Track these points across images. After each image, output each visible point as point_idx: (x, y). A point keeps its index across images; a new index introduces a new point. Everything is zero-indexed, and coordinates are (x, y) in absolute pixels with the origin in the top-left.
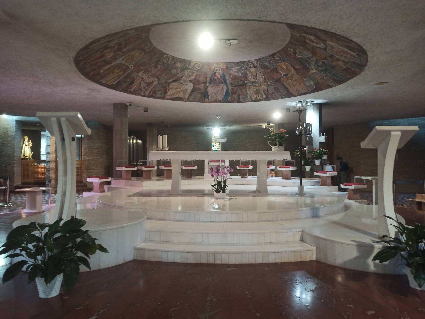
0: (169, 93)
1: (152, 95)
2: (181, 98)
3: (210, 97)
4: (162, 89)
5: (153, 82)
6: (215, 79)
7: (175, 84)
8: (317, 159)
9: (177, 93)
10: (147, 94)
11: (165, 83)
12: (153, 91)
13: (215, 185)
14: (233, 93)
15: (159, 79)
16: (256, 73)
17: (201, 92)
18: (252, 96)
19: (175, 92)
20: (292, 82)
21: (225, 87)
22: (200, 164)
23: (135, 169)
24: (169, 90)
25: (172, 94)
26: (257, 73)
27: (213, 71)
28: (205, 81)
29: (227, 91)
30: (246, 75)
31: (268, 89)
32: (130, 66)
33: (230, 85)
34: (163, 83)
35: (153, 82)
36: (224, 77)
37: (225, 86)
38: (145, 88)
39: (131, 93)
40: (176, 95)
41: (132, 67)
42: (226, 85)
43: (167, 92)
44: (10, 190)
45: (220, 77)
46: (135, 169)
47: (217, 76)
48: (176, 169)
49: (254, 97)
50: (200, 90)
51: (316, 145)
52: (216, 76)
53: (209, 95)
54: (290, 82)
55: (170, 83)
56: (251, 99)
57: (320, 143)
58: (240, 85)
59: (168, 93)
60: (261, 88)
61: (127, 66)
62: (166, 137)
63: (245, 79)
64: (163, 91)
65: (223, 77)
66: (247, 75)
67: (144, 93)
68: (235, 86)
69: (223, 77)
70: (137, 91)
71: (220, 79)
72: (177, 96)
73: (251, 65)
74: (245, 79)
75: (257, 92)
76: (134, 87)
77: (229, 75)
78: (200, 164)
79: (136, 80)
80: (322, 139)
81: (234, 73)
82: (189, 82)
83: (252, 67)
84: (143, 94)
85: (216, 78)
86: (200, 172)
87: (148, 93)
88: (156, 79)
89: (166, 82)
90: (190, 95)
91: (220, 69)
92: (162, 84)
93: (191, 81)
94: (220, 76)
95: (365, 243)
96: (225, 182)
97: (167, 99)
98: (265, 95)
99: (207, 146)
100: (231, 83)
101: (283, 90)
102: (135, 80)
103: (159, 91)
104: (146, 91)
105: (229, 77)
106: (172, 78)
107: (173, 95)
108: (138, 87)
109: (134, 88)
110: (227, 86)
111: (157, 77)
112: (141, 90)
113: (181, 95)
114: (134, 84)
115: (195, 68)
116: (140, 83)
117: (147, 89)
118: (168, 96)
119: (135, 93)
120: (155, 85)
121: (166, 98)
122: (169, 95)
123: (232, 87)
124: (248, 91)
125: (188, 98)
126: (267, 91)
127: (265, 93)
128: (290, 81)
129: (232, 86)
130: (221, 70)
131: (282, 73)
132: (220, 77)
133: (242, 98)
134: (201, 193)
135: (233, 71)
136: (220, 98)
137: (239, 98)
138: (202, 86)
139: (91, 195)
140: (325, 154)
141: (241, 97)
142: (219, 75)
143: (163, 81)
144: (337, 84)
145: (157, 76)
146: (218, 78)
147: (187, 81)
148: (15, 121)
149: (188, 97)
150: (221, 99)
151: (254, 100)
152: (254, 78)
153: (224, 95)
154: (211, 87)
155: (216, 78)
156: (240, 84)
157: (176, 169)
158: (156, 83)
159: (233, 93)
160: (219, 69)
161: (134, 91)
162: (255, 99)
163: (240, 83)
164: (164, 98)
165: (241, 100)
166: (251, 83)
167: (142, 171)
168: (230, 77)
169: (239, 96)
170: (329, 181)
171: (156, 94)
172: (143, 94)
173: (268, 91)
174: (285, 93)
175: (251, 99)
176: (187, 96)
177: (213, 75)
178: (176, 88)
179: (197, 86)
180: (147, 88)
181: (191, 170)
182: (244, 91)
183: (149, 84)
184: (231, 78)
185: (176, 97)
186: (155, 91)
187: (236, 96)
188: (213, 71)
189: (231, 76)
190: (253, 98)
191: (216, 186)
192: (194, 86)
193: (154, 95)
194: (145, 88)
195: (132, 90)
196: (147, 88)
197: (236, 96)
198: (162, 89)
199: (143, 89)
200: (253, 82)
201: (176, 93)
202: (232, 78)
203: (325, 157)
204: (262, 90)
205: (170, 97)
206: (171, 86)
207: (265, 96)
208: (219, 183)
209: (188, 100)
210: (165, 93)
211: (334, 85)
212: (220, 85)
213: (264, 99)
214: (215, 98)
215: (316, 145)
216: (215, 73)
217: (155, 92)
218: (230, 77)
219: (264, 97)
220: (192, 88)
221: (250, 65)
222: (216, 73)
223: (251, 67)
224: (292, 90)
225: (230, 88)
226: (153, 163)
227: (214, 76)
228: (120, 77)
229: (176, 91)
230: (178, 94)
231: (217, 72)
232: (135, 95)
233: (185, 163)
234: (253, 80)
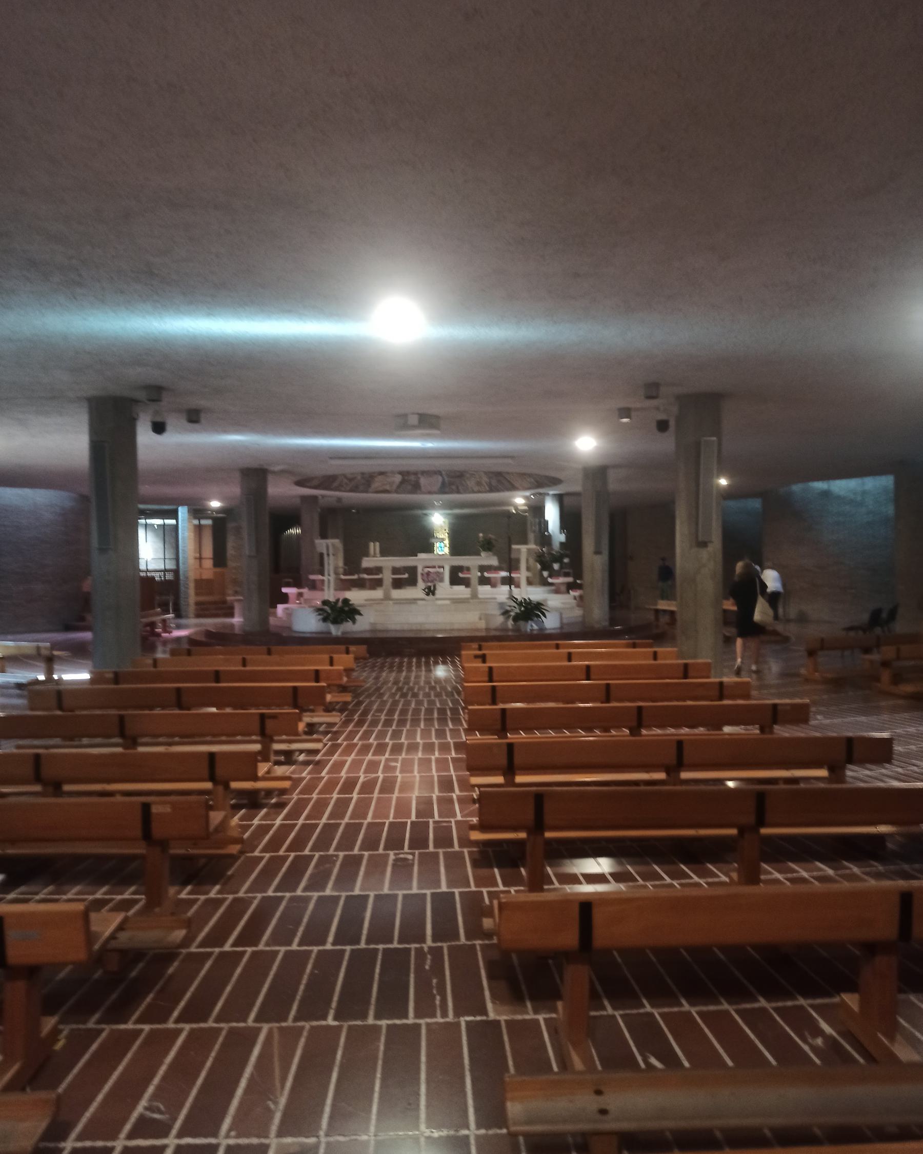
8: (556, 561)
13: (425, 589)
14: (451, 484)
22: (412, 571)
23: (355, 577)
46: (355, 577)
48: (387, 577)
49: (476, 489)
51: (556, 546)
57: (561, 544)
62: (378, 544)
75: (479, 484)
78: (412, 571)
80: (562, 538)
85: (345, 1061)
86: (412, 582)
90: (399, 487)
95: (902, 787)
96: (435, 586)
99: (424, 543)
113: (388, 488)
134: (414, 601)
136: (436, 488)
138: (412, 478)
139: (195, 638)
140: (567, 556)
141: (460, 488)
148: (391, 568)
157: (387, 577)
159: (451, 484)
164: (367, 492)
167: (364, 579)
170: (563, 588)
176: (394, 487)
179: (406, 478)
181: (400, 579)
191: (427, 590)
197: (454, 487)
203: (566, 560)
206: (376, 479)
208: (429, 588)
209: (396, 492)
215: (556, 546)
224: (517, 485)
233: (395, 571)
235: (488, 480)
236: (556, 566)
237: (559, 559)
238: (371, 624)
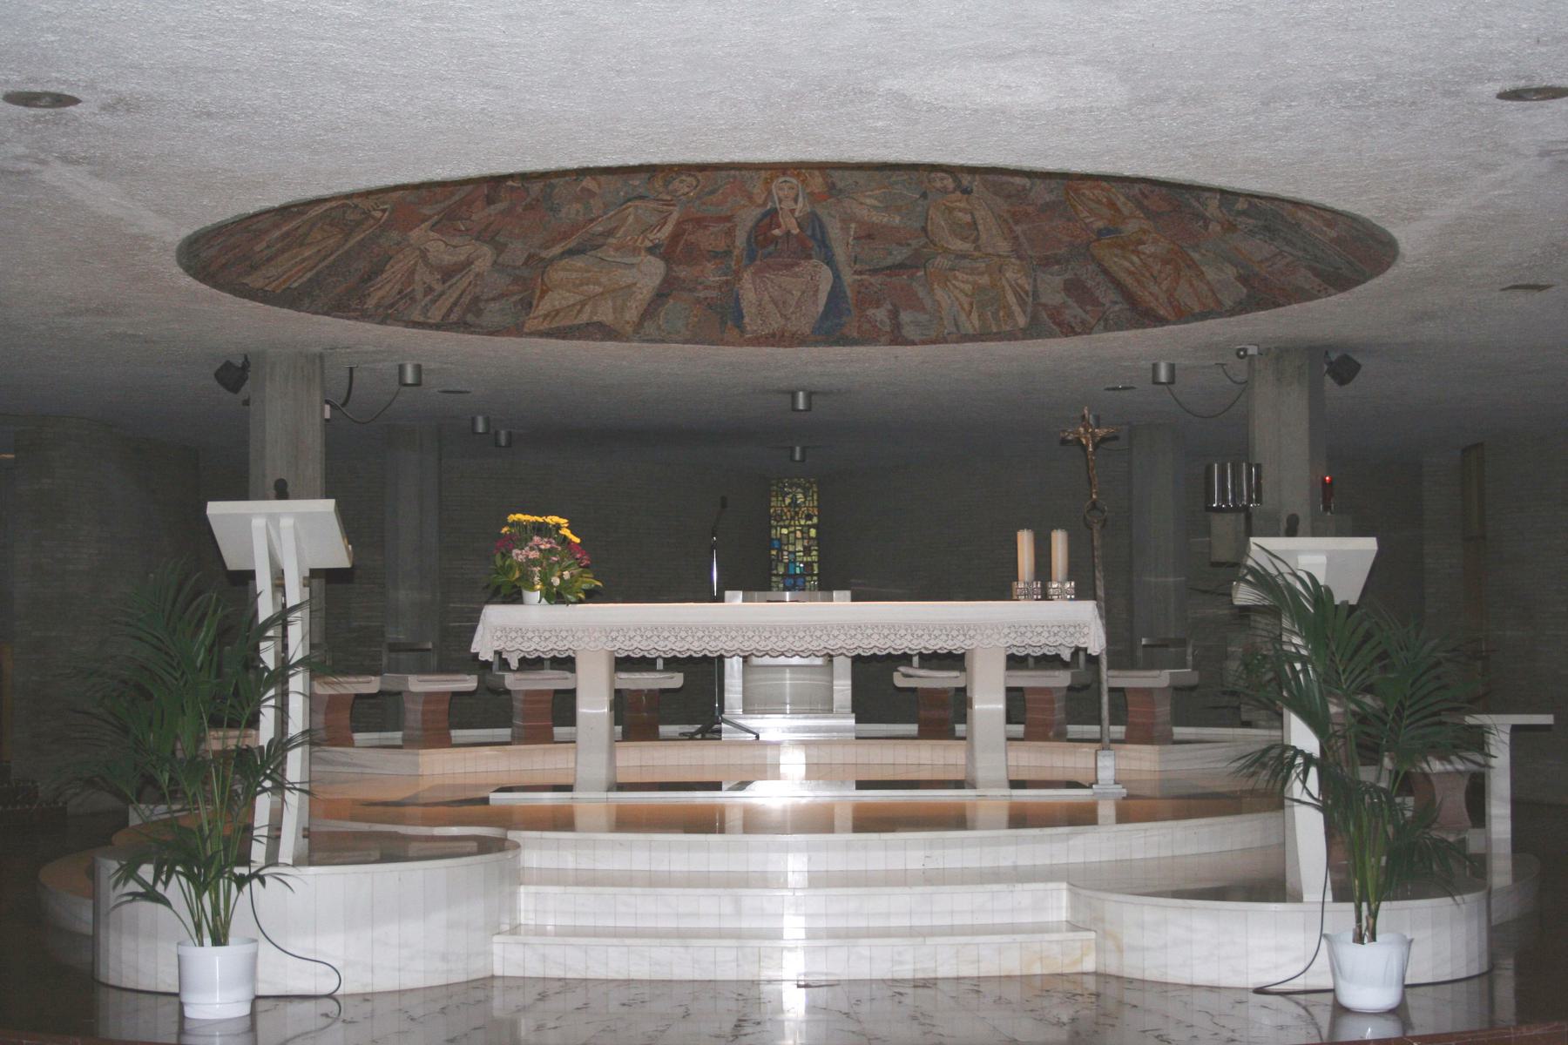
0: (545, 306)
1: (464, 320)
2: (600, 325)
3: (746, 320)
4: (511, 288)
5: (469, 263)
6: (775, 240)
7: (579, 262)
9: (583, 304)
10: (436, 315)
11: (525, 263)
12: (466, 299)
15: (500, 248)
16: (972, 214)
17: (702, 295)
18: (963, 317)
19: (572, 298)
20: (1141, 259)
21: (826, 274)
23: (371, 685)
24: (544, 293)
25: (558, 312)
26: (977, 214)
27: (765, 204)
28: (722, 245)
29: (836, 294)
30: (926, 223)
31: (1035, 286)
32: (374, 210)
33: (850, 266)
34: (519, 263)
35: (469, 263)
36: (817, 228)
37: (825, 267)
38: (429, 290)
39: (364, 316)
40: (579, 312)
41: (384, 211)
42: (827, 264)
43: (535, 303)
44: (1112, 648)
45: (796, 231)
47: (783, 227)
50: (700, 287)
52: (779, 226)
53: (744, 311)
54: (1132, 263)
55: (552, 261)
56: (957, 325)
58: (901, 266)
59: (537, 306)
60: (1003, 279)
61: (364, 213)
63: (923, 240)
64: (516, 298)
65: (814, 230)
66: (929, 222)
67: (425, 310)
68: (874, 272)
69: (814, 230)
70: (392, 305)
71: (797, 236)
72: (584, 318)
73: (945, 182)
74: (923, 240)
76: (383, 290)
77: (843, 221)
79: (392, 262)
81: (865, 212)
82: (643, 253)
83: (951, 189)
84: (421, 319)
85: (777, 232)
87: (444, 310)
88: (486, 250)
89: (530, 257)
90: (649, 312)
91: (797, 195)
92: (514, 268)
93: (651, 250)
94: (799, 225)
97: (531, 334)
98: (1024, 312)
100: (856, 257)
101: (1107, 296)
102: (387, 262)
103: (493, 299)
104: (434, 301)
105: (842, 229)
106: (565, 236)
107: (562, 314)
108: (398, 287)
109: (381, 293)
110: (832, 270)
111: (492, 241)
112: (413, 300)
113: (605, 314)
114: (384, 276)
115: (676, 191)
116: (412, 272)
117: (442, 294)
118: (536, 321)
119: (386, 315)
120: (477, 275)
121: (526, 330)
122: (546, 316)
123: (856, 273)
124: (940, 293)
125: (639, 325)
126: (1030, 294)
127: (1022, 303)
128: (1135, 259)
129: (857, 267)
130: (800, 199)
131: (1091, 222)
132: (796, 231)
133: (911, 322)
135: (861, 203)
136: (804, 326)
137: (897, 326)
142: (794, 221)
143: (517, 252)
144: (1331, 290)
145: (492, 238)
146: (788, 233)
147: (635, 251)
149: (636, 319)
150: (807, 330)
151: (971, 331)
152: (964, 239)
153: (821, 309)
154: (755, 274)
155: (777, 232)
156: (899, 258)
158: (483, 263)
160: (792, 194)
161: (378, 306)
162: (975, 330)
163: (899, 255)
164: (517, 330)
165: (909, 331)
166: (953, 257)
168: (849, 228)
169: (894, 314)
171: (479, 313)
172: (416, 316)
173: (1035, 294)
174: (1117, 308)
175: (957, 325)
176: (632, 315)
177: (761, 220)
178: (581, 284)
180: (438, 288)
182: (921, 295)
183: (447, 274)
184: (852, 233)
185: (576, 322)
186: (476, 300)
187: (880, 314)
188: (765, 204)
189: (853, 225)
190: (968, 325)
192: (669, 269)
193: (470, 318)
194: (429, 290)
195: (370, 303)
196: (438, 288)
197: (880, 314)
198: (511, 288)
199: (419, 296)
200: (964, 256)
201: (578, 307)
202: (855, 232)
204: (1007, 287)
205: (545, 326)
206: (556, 275)
207: (1026, 316)
209: (638, 332)
210: (527, 305)
211: (1319, 291)
212: (798, 264)
213: (1021, 329)
214: (776, 323)
216: (773, 213)
217: (475, 306)
218: (845, 229)
219: (1022, 321)
220: (657, 281)
221: (942, 179)
222: (780, 212)
223: (945, 187)
225: (848, 277)
226: (1261, 847)
227: (771, 224)
228: (325, 258)
229: (578, 298)
230: (588, 309)
231: (781, 209)
232: (383, 322)
234: (958, 245)
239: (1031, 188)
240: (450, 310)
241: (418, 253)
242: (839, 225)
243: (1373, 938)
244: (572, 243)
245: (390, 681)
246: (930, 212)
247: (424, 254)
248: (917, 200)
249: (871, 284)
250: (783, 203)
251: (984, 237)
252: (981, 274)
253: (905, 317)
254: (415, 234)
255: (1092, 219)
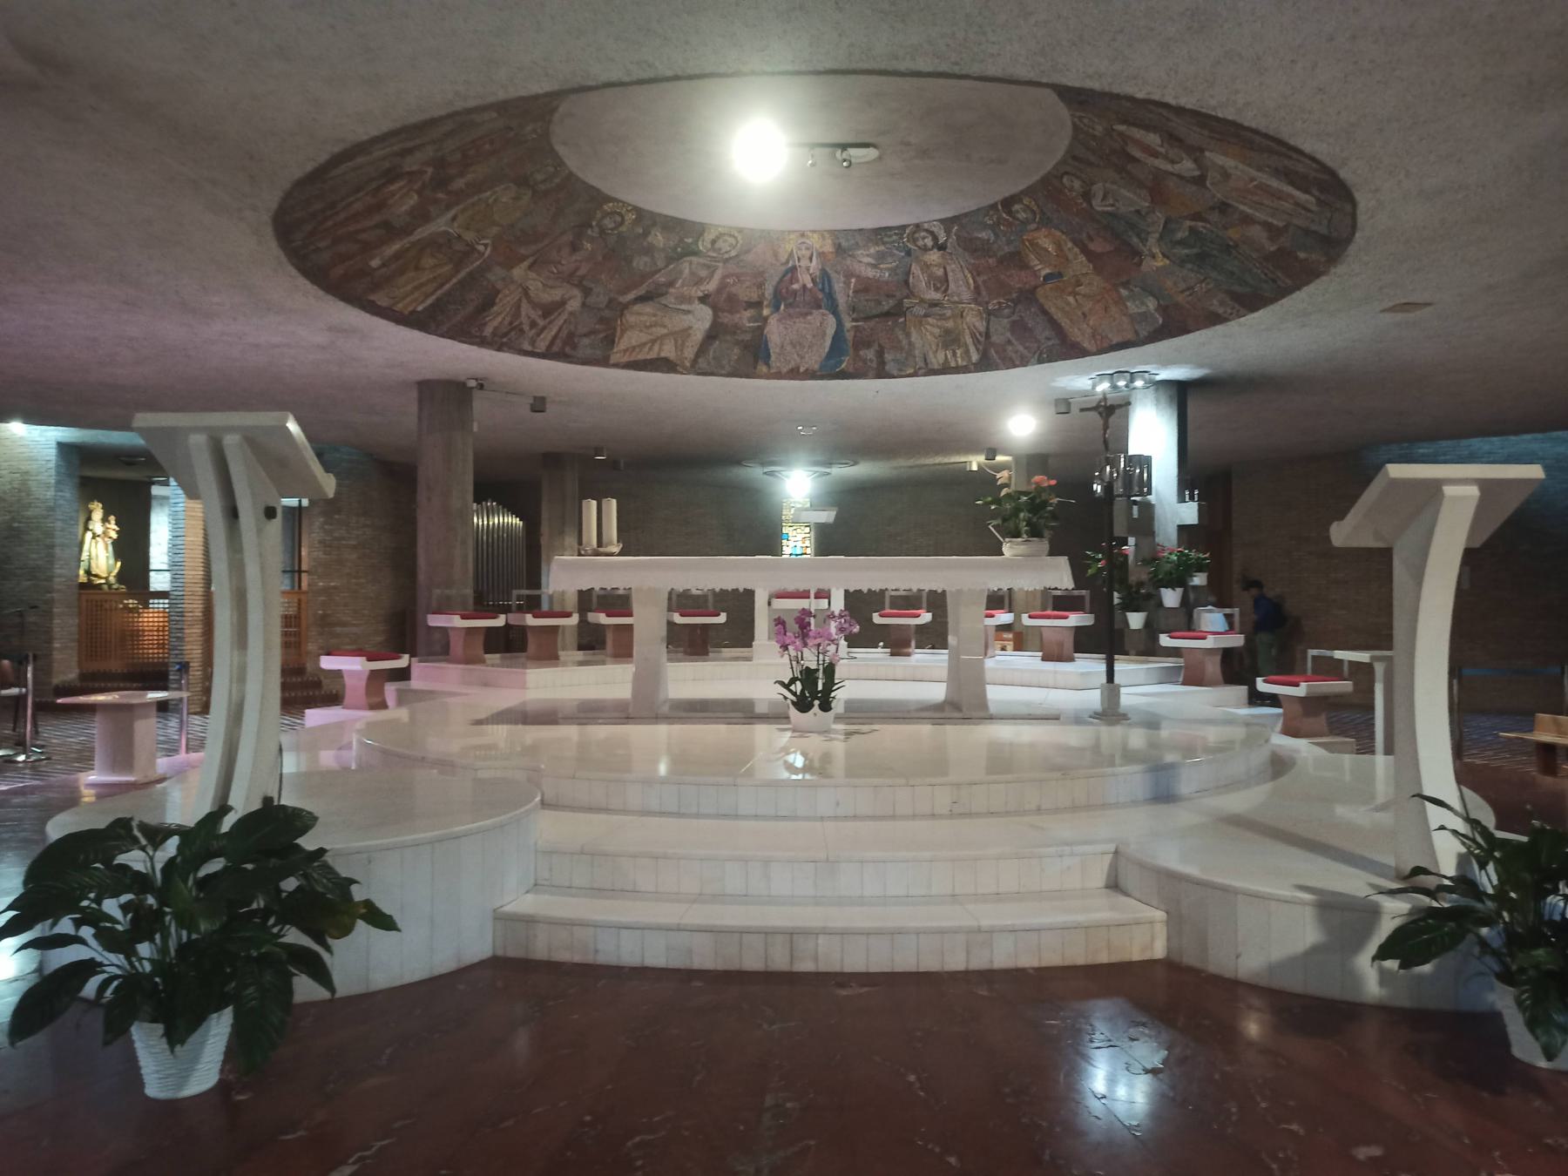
0: (623, 343)
1: (562, 351)
2: (666, 360)
3: (773, 357)
4: (597, 327)
5: (563, 303)
6: (795, 293)
8: (1171, 584)
9: (653, 342)
10: (542, 346)
11: (607, 306)
12: (564, 334)
13: (793, 681)
14: (861, 343)
15: (587, 292)
17: (740, 338)
18: (931, 355)
19: (644, 337)
20: (1076, 301)
21: (831, 321)
22: (740, 604)
23: (500, 622)
24: (623, 332)
25: (634, 348)
27: (787, 262)
28: (755, 297)
29: (838, 337)
31: (988, 328)
32: (478, 244)
33: (849, 314)
35: (563, 303)
36: (826, 282)
37: (831, 316)
38: (533, 324)
39: (482, 342)
41: (486, 245)
42: (833, 313)
45: (810, 285)
46: (500, 622)
47: (801, 281)
48: (648, 622)
49: (937, 359)
50: (739, 331)
51: (1167, 535)
52: (798, 281)
53: (771, 351)
54: (1068, 304)
55: (626, 306)
56: (926, 364)
57: (1182, 529)
58: (887, 314)
59: (619, 342)
61: (468, 245)
62: (612, 505)
63: (906, 292)
64: (602, 335)
66: (911, 276)
67: (533, 342)
68: (867, 318)
69: (823, 284)
70: (505, 335)
71: (810, 290)
72: (653, 355)
73: (926, 240)
74: (906, 292)
75: (950, 340)
76: (495, 321)
78: (740, 604)
79: (500, 296)
80: (1189, 513)
81: (863, 268)
82: (697, 302)
83: (930, 247)
84: (529, 348)
85: (795, 286)
86: (740, 634)
87: (547, 343)
88: (576, 292)
89: (611, 301)
90: (702, 350)
91: (812, 255)
92: (599, 309)
93: (703, 299)
94: (813, 280)
95: (1348, 896)
96: (830, 670)
97: (616, 366)
98: (978, 350)
99: (765, 540)
100: (854, 307)
101: (1043, 332)
102: (496, 296)
103: (585, 335)
104: (538, 335)
106: (635, 286)
107: (637, 350)
108: (508, 319)
109: (495, 323)
110: (836, 319)
112: (522, 331)
113: (668, 351)
114: (495, 308)
116: (518, 306)
117: (544, 328)
118: (618, 355)
119: (499, 342)
120: (571, 313)
121: (612, 362)
122: (625, 351)
123: (854, 320)
125: (695, 361)
126: (984, 335)
127: (976, 342)
128: (1071, 299)
129: (855, 316)
130: (814, 258)
131: (1039, 270)
132: (810, 285)
133: (893, 360)
134: (742, 712)
135: (860, 262)
136: (813, 360)
137: (882, 363)
138: (745, 318)
139: (336, 721)
140: (1200, 568)
142: (809, 276)
143: (600, 298)
144: (1242, 311)
145: (580, 282)
146: (804, 286)
147: (689, 300)
148: (54, 445)
150: (816, 367)
151: (936, 367)
153: (827, 350)
154: (779, 320)
155: (795, 286)
156: (886, 308)
157: (648, 622)
158: (574, 305)
159: (861, 343)
160: (808, 253)
161: (494, 334)
162: (939, 365)
164: (604, 362)
165: (890, 367)
166: (926, 306)
167: (523, 630)
168: (850, 282)
169: (880, 353)
170: (1213, 667)
171: (574, 347)
172: (527, 347)
173: (987, 335)
174: (1050, 343)
176: (689, 353)
177: (784, 276)
178: (651, 326)
179: (726, 318)
180: (541, 323)
181: (705, 627)
182: (901, 337)
184: (852, 287)
185: (649, 357)
186: (571, 335)
187: (869, 354)
188: (787, 262)
189: (853, 280)
190: (934, 360)
192: (715, 316)
193: (567, 350)
194: (533, 324)
195: (488, 331)
196: (541, 323)
197: (869, 354)
198: (597, 327)
199: (526, 327)
200: (934, 304)
201: (650, 345)
202: (854, 286)
203: (1199, 580)
204: (967, 331)
205: (626, 359)
206: (630, 318)
207: (979, 353)
208: (808, 676)
209: (695, 369)
210: (610, 341)
211: (1231, 314)
212: (811, 314)
214: (794, 360)
215: (1167, 535)
216: (794, 269)
217: (571, 340)
218: (847, 284)
219: (975, 357)
220: (707, 325)
221: (924, 238)
222: (799, 269)
223: (925, 245)
224: (1078, 334)
225: (848, 324)
227: (791, 280)
228: (442, 285)
229: (650, 337)
230: (656, 348)
231: (800, 266)
232: (499, 350)
233: (683, 601)
234: (933, 295)
235: (981, 326)
236: (1171, 598)
237: (1177, 579)
238: (504, 920)
239: (994, 242)
240: (552, 343)
241: (520, 289)
242: (842, 279)
243: (670, 593)
244: (641, 291)
245: (514, 619)
246: (913, 267)
247: (526, 292)
248: (903, 257)
249: (864, 329)
250: (801, 261)
251: (952, 286)
252: (947, 319)
253: (888, 357)
254: (518, 272)
255: (1039, 267)
